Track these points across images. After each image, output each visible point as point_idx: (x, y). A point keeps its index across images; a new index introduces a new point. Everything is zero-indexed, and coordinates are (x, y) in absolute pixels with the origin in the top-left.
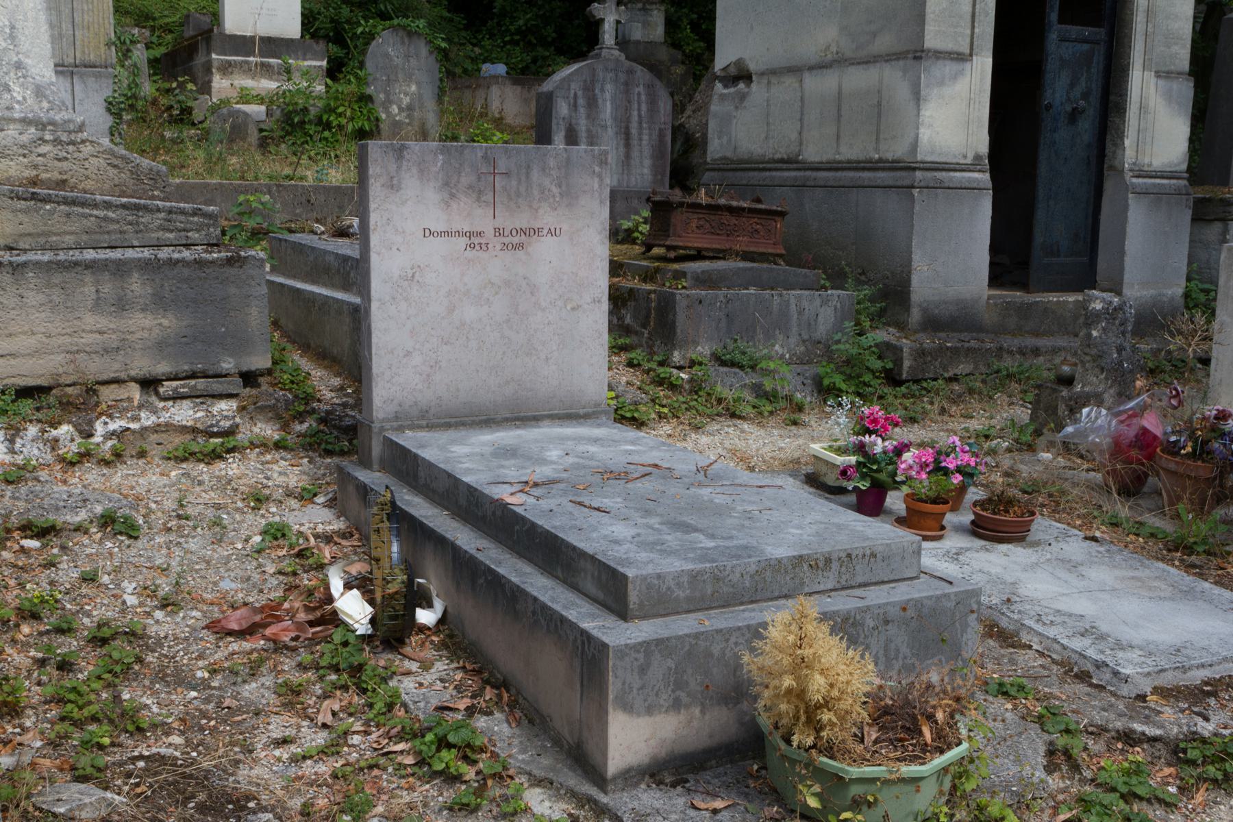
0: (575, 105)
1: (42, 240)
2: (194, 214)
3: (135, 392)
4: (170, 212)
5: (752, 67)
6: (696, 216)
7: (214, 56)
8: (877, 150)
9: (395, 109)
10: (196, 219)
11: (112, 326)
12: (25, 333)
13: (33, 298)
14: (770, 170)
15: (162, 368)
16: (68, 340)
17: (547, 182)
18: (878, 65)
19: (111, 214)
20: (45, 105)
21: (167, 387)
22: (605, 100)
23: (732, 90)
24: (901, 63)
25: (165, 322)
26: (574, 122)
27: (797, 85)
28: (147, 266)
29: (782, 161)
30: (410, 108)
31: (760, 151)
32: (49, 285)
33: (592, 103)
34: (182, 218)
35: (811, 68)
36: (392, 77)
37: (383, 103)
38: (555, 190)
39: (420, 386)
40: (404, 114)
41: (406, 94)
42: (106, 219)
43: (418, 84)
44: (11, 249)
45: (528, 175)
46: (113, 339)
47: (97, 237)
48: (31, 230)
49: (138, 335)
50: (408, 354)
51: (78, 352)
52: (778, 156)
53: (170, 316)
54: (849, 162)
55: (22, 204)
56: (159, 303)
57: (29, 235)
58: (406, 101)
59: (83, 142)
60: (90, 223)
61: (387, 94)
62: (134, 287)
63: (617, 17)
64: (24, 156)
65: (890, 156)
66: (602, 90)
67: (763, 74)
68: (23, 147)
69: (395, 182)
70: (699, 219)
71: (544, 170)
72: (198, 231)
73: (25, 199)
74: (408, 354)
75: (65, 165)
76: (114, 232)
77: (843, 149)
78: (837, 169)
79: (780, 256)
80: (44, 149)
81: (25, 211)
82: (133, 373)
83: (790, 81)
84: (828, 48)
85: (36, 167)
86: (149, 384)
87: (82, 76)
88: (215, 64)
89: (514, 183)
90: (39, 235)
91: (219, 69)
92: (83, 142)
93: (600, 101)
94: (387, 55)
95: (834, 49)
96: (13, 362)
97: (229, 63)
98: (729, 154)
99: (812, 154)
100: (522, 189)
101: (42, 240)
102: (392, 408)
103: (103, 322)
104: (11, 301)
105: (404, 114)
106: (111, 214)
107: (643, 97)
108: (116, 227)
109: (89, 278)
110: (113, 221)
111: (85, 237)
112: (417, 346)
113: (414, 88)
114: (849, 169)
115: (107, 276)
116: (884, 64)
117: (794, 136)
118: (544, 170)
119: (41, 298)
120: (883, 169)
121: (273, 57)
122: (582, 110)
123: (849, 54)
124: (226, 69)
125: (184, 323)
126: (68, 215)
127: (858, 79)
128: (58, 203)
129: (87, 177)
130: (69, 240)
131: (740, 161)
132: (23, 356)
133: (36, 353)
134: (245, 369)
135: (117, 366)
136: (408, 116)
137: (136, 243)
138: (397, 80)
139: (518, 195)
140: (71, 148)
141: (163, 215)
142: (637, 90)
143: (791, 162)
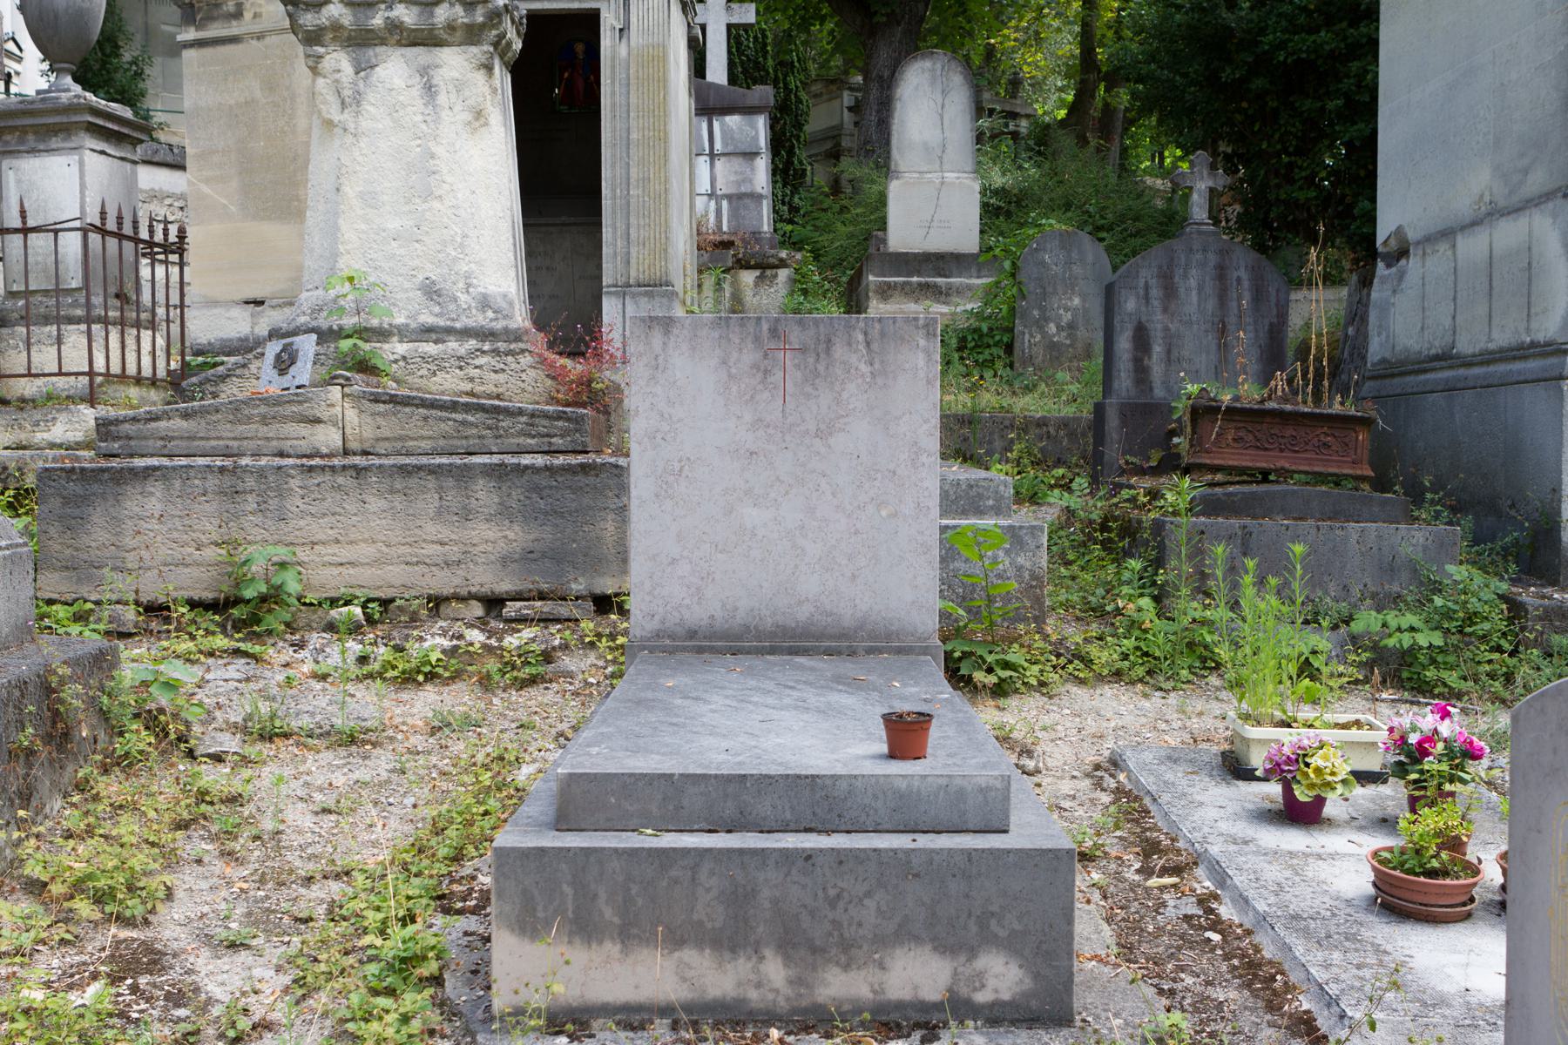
0: (1147, 298)
1: (399, 445)
2: (559, 418)
3: (477, 610)
4: (532, 415)
5: (1412, 235)
6: (1233, 425)
7: (871, 278)
8: (1528, 330)
9: (1052, 328)
10: (560, 423)
11: (453, 537)
12: (365, 541)
13: (375, 504)
14: (1425, 371)
15: (505, 587)
16: (408, 550)
17: (854, 359)
18: (1527, 212)
19: (470, 418)
20: (490, 314)
21: (511, 609)
22: (1188, 289)
23: (1394, 269)
24: (1550, 205)
25: (511, 535)
26: (1144, 319)
27: (1450, 253)
28: (498, 473)
29: (1437, 358)
30: (1072, 326)
31: (1417, 348)
32: (392, 491)
33: (1170, 291)
34: (545, 422)
35: (1463, 228)
36: (1049, 289)
37: (1037, 322)
38: (864, 368)
39: (687, 601)
40: (1064, 334)
41: (1067, 309)
42: (464, 423)
43: (1084, 297)
44: (368, 453)
45: (828, 351)
46: (454, 552)
47: (455, 442)
48: (388, 434)
49: (481, 548)
50: (673, 561)
51: (418, 563)
52: (1433, 352)
53: (516, 527)
54: (1501, 350)
55: (381, 407)
56: (504, 513)
57: (387, 439)
58: (1067, 317)
59: (523, 351)
60: (447, 427)
61: (1042, 309)
62: (480, 495)
63: (1211, 184)
64: (461, 368)
65: (1541, 337)
66: (1185, 276)
67: (1418, 243)
68: (460, 358)
69: (660, 360)
70: (1238, 429)
71: (849, 344)
72: (562, 436)
73: (384, 402)
74: (673, 561)
75: (501, 377)
76: (472, 436)
77: (1495, 335)
78: (1488, 363)
79: (1363, 479)
80: (482, 360)
81: (383, 415)
82: (474, 590)
83: (1443, 247)
84: (1482, 196)
85: (472, 380)
86: (493, 603)
87: (634, 296)
88: (872, 287)
89: (811, 360)
90: (396, 439)
91: (876, 292)
92: (523, 351)
93: (1182, 290)
94: (1043, 263)
95: (1487, 199)
96: (351, 571)
97: (888, 285)
98: (1388, 355)
99: (1466, 345)
100: (821, 368)
101: (399, 445)
102: (652, 626)
103: (445, 533)
104: (351, 507)
105: (1064, 334)
106: (470, 418)
107: (1246, 284)
108: (475, 431)
109: (431, 482)
110: (471, 424)
111: (442, 442)
112: (685, 553)
113: (1077, 301)
114: (1501, 360)
115: (450, 482)
116: (1534, 210)
117: (1448, 322)
118: (849, 344)
119: (383, 504)
120: (1534, 356)
121: (941, 276)
122: (1156, 303)
123: (1502, 203)
124: (885, 292)
125: (532, 537)
126: (425, 419)
127: (1508, 233)
128: (417, 406)
129: (523, 390)
130: (426, 445)
131: (1402, 363)
132: (362, 564)
133: (376, 562)
134: (598, 591)
135: (457, 581)
136: (1069, 336)
137: (494, 449)
138: (1055, 293)
139: (816, 374)
140: (510, 359)
141: (524, 419)
142: (1235, 274)
143: (1445, 358)
